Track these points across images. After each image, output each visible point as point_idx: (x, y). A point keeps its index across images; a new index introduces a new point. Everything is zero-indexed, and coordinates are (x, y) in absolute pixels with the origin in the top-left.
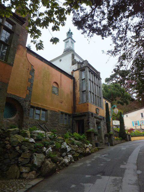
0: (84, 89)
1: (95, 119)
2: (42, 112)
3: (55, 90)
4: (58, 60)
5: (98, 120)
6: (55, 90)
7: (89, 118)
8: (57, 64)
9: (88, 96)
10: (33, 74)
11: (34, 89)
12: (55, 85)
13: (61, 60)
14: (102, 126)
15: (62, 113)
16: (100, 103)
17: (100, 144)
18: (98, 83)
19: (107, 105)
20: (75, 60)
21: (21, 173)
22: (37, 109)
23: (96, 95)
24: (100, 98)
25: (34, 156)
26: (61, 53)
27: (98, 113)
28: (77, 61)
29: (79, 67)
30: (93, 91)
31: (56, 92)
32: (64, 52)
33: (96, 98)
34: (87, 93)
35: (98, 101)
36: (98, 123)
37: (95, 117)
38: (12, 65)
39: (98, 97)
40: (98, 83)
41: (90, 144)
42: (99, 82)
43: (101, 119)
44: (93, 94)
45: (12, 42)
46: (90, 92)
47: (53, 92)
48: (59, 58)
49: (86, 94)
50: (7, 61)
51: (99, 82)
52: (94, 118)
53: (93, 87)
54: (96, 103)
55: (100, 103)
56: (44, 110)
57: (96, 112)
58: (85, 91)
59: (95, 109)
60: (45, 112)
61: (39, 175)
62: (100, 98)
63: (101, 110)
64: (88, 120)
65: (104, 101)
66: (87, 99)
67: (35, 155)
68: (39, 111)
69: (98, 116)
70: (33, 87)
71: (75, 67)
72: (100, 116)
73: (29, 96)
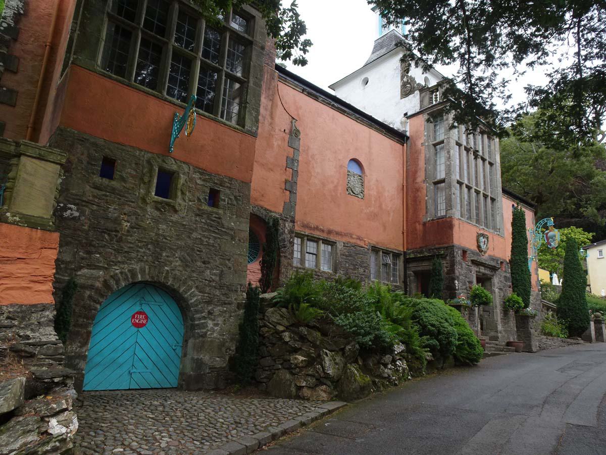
0: (441, 175)
1: (474, 269)
2: (322, 247)
3: (355, 182)
4: (358, 82)
5: (482, 270)
6: (355, 182)
7: (452, 264)
8: (351, 95)
9: (453, 196)
10: (297, 143)
11: (302, 191)
12: (355, 170)
13: (366, 82)
14: (497, 290)
15: (375, 250)
16: (493, 215)
17: (490, 344)
18: (486, 149)
19: (518, 222)
20: (412, 80)
21: (300, 388)
22: (308, 240)
23: (477, 192)
24: (493, 200)
25: (325, 356)
26: (365, 53)
27: (483, 247)
28: (419, 84)
29: (426, 104)
30: (469, 179)
31: (357, 190)
32: (374, 48)
33: (478, 201)
34: (450, 187)
35: (486, 211)
36: (483, 280)
37: (474, 262)
38: (254, 135)
39: (485, 196)
40: (486, 149)
41: (487, 35)
42: (489, 146)
43: (494, 269)
44: (469, 188)
45: (252, 71)
46: (460, 183)
47: (350, 190)
48: (361, 74)
49: (447, 190)
50: (244, 127)
51: (489, 146)
52: (470, 264)
53: (468, 166)
54: (478, 215)
55: (493, 215)
56: (326, 242)
57: (479, 247)
58: (443, 181)
59: (475, 235)
60: (330, 247)
61: (336, 396)
62: (493, 200)
63: (496, 238)
64: (452, 270)
65: (506, 207)
66: (449, 206)
67: (327, 354)
68: (315, 244)
69: (484, 258)
70: (300, 181)
71: (413, 103)
72: (493, 258)
73: (290, 206)
